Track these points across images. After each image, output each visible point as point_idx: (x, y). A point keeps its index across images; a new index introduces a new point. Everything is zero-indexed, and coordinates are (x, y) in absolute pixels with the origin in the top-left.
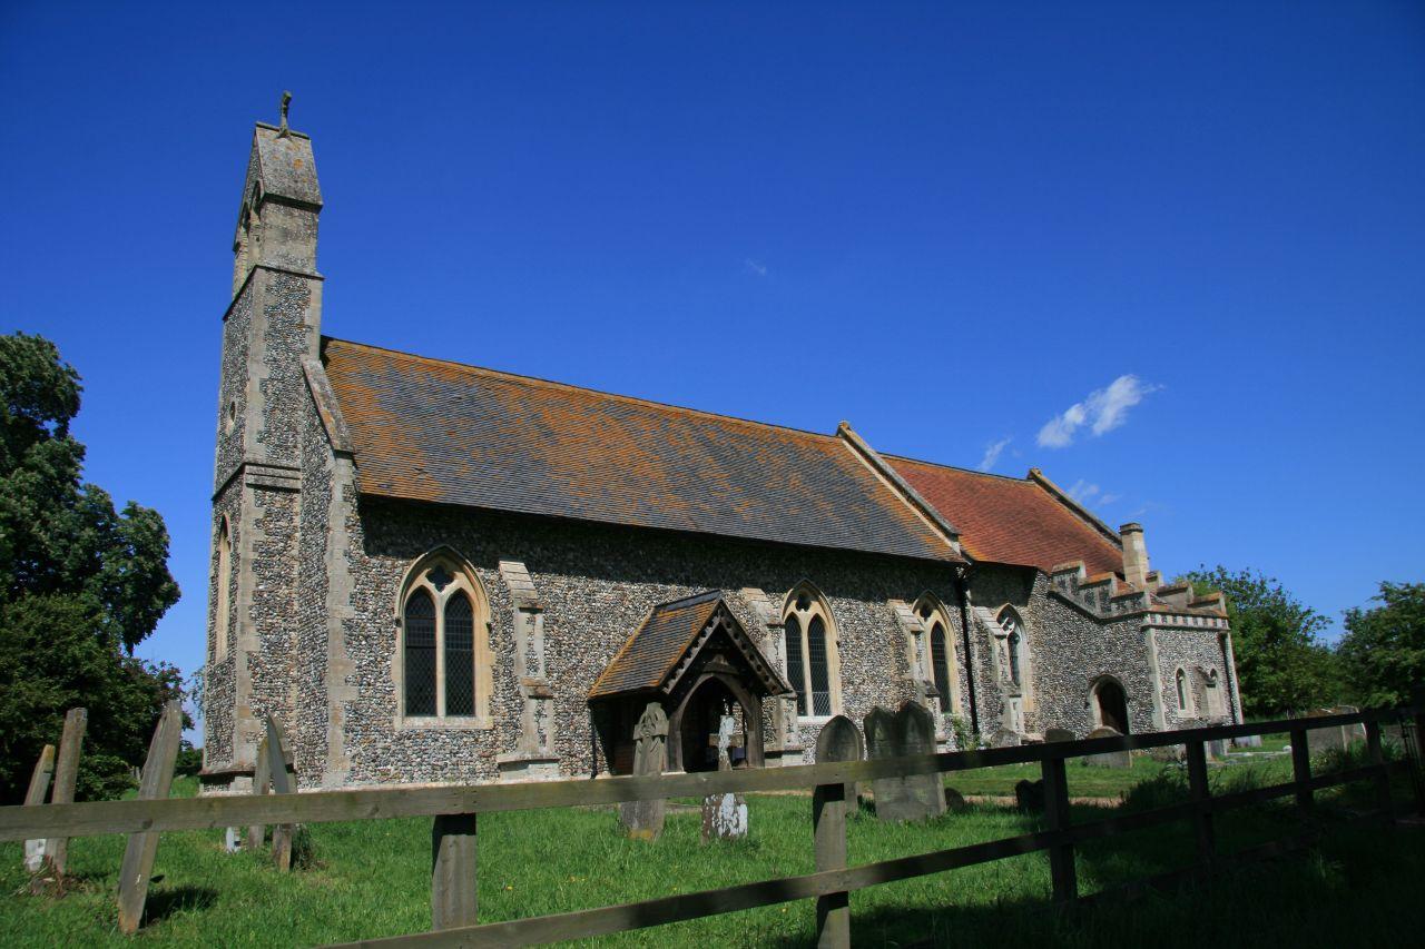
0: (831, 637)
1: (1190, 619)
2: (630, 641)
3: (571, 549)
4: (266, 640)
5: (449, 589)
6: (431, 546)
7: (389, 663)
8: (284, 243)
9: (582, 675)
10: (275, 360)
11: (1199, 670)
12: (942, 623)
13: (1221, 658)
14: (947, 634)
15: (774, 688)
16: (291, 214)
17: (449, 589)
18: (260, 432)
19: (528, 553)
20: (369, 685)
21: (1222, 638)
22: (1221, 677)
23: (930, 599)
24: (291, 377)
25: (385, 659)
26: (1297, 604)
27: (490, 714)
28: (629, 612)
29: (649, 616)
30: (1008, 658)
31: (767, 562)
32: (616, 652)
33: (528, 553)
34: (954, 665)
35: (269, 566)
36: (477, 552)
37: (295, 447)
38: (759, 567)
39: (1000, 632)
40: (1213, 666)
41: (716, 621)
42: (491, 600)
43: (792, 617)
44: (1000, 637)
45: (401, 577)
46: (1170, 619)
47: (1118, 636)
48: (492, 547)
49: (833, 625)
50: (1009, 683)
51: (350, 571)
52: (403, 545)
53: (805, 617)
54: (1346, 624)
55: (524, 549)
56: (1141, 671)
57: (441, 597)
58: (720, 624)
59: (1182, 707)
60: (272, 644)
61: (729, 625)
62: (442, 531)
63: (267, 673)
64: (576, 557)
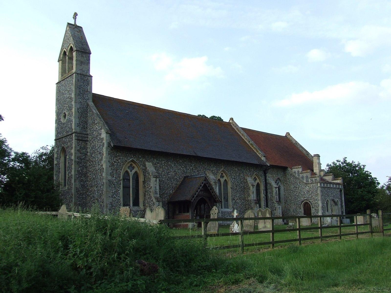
0: (229, 186)
1: (329, 185)
2: (178, 186)
3: (163, 160)
4: (81, 184)
5: (134, 171)
6: (129, 159)
7: (119, 191)
8: (81, 65)
9: (166, 195)
10: (81, 102)
11: (333, 200)
12: (259, 182)
13: (340, 197)
14: (260, 186)
15: (218, 201)
16: (83, 56)
17: (134, 171)
18: (77, 124)
19: (153, 161)
20: (115, 197)
21: (341, 191)
22: (339, 203)
23: (223, 172)
24: (85, 107)
25: (119, 190)
26: (16, 211)
27: (143, 206)
28: (178, 178)
29: (182, 179)
30: (278, 194)
31: (213, 164)
32: (174, 189)
33: (153, 161)
34: (262, 195)
35: (81, 163)
36: (140, 161)
37: (87, 128)
38: (211, 166)
39: (276, 186)
40: (337, 199)
41: (204, 182)
42: (144, 174)
43: (219, 180)
44: (276, 188)
45: (122, 168)
46: (326, 185)
47: (310, 189)
48: (144, 160)
49: (230, 183)
50: (278, 201)
51: (110, 166)
52: (122, 159)
53: (222, 180)
54: (222, 178)
55: (152, 160)
56: (316, 200)
57: (131, 174)
58: (205, 183)
59: (328, 211)
60: (82, 185)
61: (207, 183)
62: (132, 155)
63: (81, 193)
64: (165, 162)
